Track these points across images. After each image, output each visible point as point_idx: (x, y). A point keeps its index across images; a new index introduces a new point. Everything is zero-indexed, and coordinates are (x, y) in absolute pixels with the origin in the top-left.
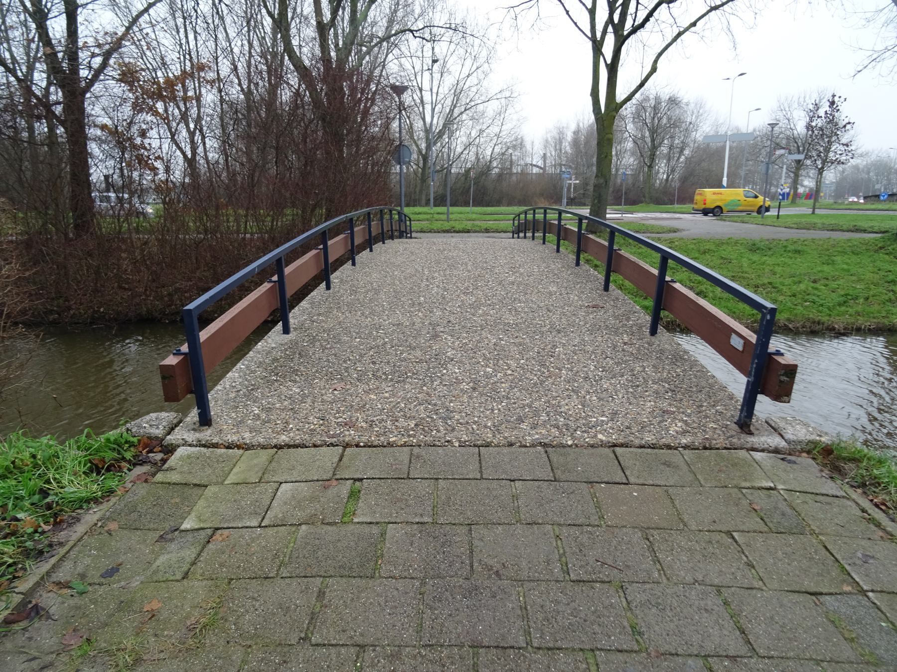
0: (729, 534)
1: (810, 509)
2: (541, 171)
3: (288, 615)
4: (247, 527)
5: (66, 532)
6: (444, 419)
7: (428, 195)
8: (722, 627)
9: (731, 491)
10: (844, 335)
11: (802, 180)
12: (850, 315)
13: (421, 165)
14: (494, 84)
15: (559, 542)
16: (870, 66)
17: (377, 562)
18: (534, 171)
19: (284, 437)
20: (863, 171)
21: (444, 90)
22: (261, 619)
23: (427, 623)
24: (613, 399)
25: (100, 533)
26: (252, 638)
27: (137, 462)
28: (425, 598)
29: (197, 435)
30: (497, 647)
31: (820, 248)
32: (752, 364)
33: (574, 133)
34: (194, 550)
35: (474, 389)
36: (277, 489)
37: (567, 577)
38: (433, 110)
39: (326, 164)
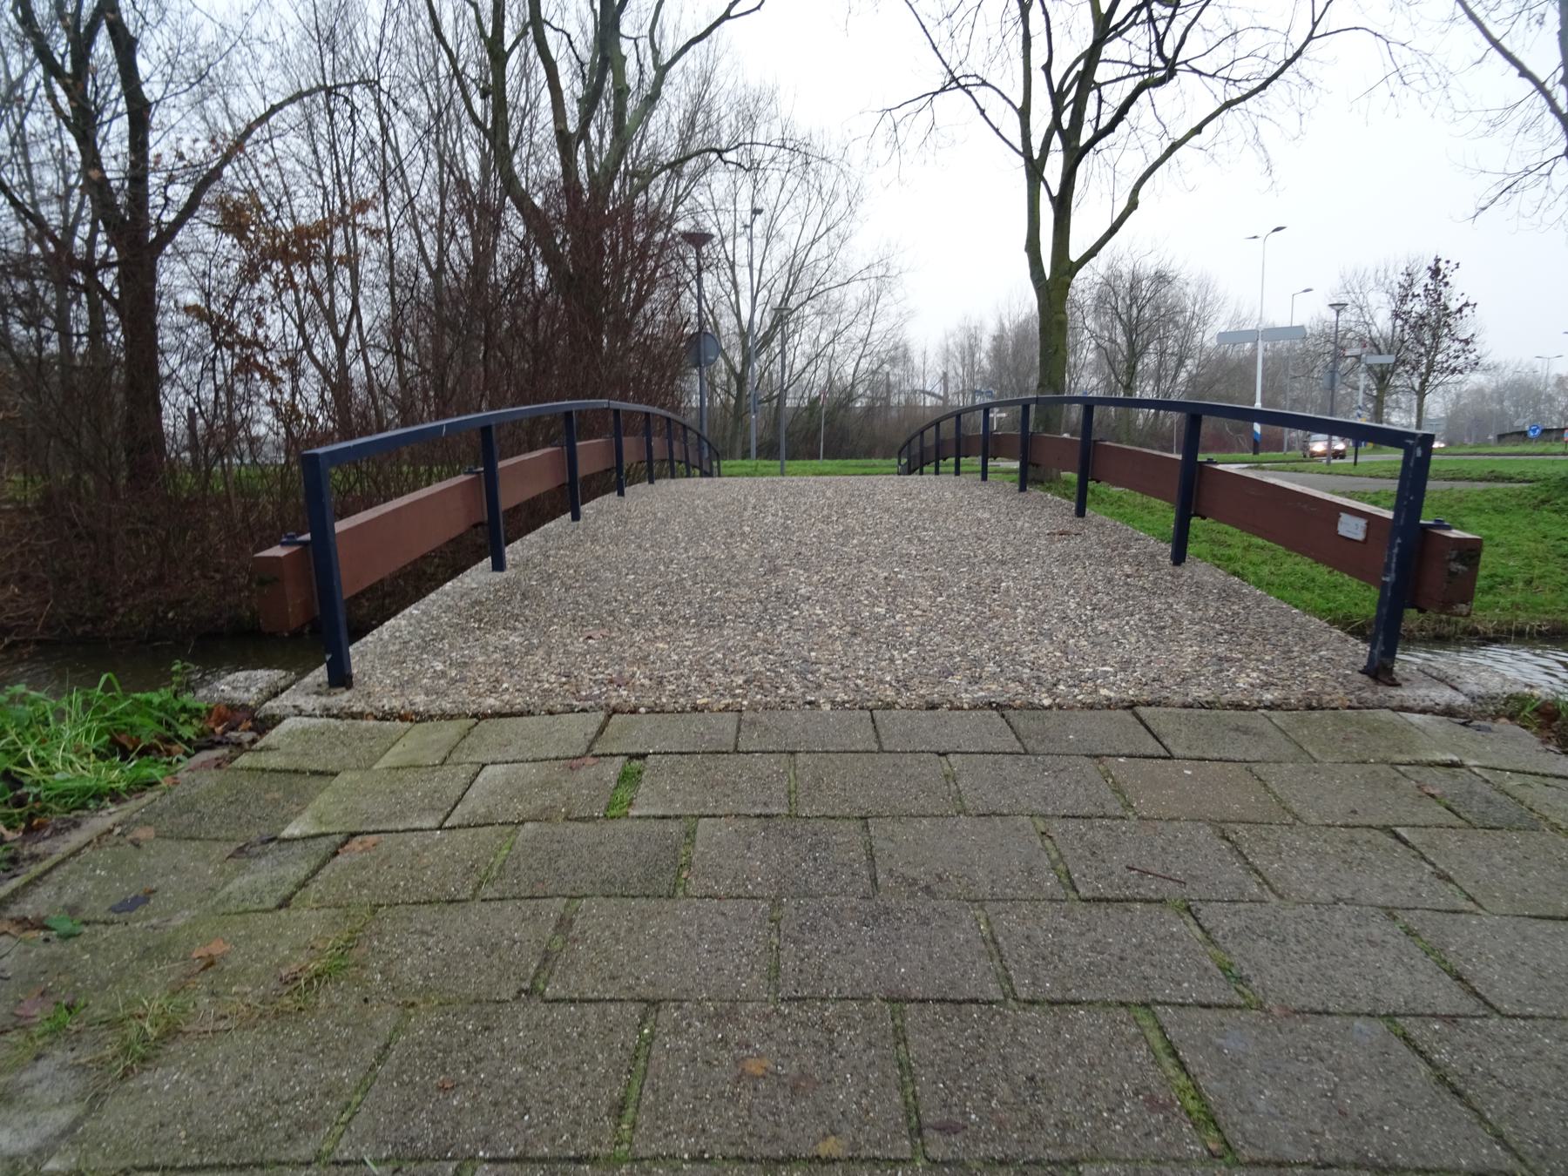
0: (1389, 830)
1: (1538, 794)
2: (940, 402)
3: (496, 955)
4: (414, 830)
5: (48, 842)
6: (801, 675)
7: (746, 442)
8: (1411, 970)
9: (1377, 768)
10: (1495, 641)
11: (1389, 414)
12: (1503, 609)
13: (734, 390)
14: (858, 252)
15: (1048, 842)
16: (1501, 199)
17: (679, 875)
18: (928, 404)
19: (491, 701)
20: (1491, 397)
21: (772, 266)
22: (438, 964)
23: (789, 965)
24: (1120, 644)
25: (117, 844)
26: (417, 993)
27: (206, 742)
28: (782, 927)
29: (324, 700)
30: (942, 1001)
31: (1436, 504)
32: (1391, 548)
33: (995, 338)
34: (305, 866)
35: (854, 634)
36: (477, 774)
37: (1072, 895)
38: (754, 299)
39: (571, 340)
